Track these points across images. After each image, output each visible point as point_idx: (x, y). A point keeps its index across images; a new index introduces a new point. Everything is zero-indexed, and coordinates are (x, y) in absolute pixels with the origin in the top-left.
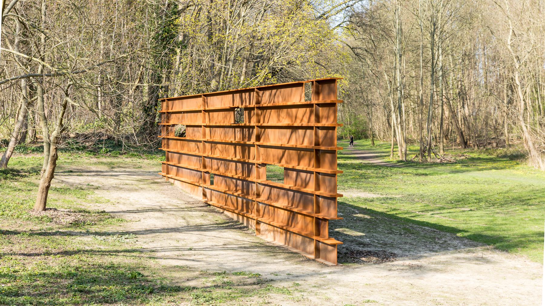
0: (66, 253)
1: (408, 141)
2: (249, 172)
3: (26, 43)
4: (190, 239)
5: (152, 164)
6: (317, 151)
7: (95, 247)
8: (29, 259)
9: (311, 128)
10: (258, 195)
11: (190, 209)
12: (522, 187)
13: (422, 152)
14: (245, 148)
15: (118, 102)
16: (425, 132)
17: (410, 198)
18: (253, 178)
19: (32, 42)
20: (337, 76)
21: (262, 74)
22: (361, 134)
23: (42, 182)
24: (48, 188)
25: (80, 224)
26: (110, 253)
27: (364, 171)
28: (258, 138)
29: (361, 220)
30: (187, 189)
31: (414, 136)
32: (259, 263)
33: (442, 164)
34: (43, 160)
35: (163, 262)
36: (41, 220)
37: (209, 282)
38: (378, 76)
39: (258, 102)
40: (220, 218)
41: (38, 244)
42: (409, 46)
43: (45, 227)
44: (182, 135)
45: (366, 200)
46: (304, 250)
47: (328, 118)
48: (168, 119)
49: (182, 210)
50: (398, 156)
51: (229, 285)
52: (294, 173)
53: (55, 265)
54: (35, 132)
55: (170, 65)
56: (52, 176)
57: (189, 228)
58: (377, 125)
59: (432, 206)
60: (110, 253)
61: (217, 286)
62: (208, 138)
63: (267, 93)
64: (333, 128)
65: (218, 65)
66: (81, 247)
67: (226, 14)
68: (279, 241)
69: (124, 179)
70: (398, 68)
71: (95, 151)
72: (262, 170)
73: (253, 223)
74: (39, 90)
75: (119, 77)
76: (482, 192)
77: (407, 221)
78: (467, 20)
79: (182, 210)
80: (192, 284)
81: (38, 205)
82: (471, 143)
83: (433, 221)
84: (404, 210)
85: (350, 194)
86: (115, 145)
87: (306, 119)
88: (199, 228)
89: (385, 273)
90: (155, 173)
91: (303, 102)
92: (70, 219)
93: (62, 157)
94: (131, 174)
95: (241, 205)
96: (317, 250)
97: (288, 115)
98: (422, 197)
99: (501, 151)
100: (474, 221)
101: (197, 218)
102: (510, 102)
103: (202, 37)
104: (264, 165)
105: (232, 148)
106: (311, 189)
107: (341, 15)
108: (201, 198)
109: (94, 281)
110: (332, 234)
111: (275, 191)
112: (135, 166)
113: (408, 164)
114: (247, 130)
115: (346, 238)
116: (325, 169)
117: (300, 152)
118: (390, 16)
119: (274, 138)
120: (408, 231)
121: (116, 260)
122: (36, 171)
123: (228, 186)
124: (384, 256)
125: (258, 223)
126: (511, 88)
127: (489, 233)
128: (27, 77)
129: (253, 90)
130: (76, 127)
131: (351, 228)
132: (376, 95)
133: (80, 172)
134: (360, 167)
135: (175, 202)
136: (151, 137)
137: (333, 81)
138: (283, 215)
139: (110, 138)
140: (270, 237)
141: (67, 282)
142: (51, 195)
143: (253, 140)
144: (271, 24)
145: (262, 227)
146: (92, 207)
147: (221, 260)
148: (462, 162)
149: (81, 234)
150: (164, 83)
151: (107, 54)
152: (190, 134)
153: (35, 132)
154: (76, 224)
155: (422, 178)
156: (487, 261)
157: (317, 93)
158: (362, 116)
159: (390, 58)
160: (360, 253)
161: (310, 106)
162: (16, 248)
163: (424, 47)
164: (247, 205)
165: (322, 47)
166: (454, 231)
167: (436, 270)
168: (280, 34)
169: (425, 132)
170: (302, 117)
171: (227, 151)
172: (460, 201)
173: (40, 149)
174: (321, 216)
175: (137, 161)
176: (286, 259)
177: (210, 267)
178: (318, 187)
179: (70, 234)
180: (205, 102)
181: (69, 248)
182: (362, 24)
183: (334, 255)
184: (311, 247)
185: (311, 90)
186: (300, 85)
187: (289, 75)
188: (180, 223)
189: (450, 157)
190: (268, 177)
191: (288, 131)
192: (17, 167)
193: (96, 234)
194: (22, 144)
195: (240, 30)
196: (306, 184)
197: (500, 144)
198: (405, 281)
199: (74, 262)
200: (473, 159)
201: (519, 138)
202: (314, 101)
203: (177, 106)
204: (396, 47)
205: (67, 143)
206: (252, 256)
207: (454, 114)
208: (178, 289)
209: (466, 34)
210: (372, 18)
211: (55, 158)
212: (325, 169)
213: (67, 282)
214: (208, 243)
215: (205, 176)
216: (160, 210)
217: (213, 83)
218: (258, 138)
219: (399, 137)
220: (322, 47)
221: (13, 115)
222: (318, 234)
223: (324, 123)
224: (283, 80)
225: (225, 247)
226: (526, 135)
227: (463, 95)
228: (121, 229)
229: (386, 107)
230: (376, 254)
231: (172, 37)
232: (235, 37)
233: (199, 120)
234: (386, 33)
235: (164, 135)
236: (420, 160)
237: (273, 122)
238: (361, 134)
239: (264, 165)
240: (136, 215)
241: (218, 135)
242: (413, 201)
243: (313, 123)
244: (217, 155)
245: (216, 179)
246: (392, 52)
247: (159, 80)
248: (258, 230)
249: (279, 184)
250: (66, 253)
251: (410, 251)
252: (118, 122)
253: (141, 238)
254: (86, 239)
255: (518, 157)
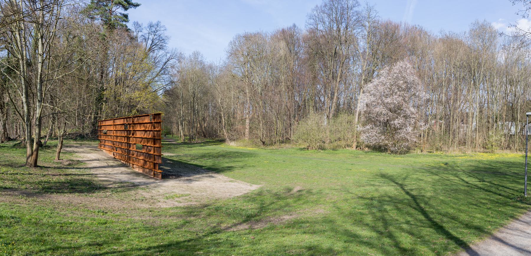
0: (66, 175)
1: (185, 135)
2: (130, 147)
3: (52, 102)
4: (109, 170)
5: (95, 144)
6: (154, 139)
7: (76, 173)
8: (54, 177)
9: (152, 131)
10: (133, 155)
11: (109, 160)
12: (223, 151)
13: (190, 139)
14: (128, 138)
15: (83, 122)
16: (191, 132)
17: (186, 156)
18: (131, 149)
19: (54, 101)
20: (160, 112)
21: (134, 111)
22: (169, 133)
23: (58, 150)
24: (60, 152)
25: (72, 164)
26: (81, 175)
27: (170, 147)
28: (133, 135)
29: (169, 163)
30: (108, 153)
31: (187, 134)
32: (133, 179)
33: (197, 143)
34: (58, 142)
35: (100, 179)
36: (58, 163)
37: (116, 185)
38: (175, 112)
39: (133, 122)
40: (119, 163)
41: (57, 171)
42: (185, 102)
43: (59, 165)
44: (105, 133)
45: (171, 156)
46: (150, 174)
47: (158, 127)
48: (101, 128)
49: (106, 160)
50: (182, 141)
51: (122, 187)
52: (146, 147)
53: (63, 179)
54: (55, 133)
55: (101, 109)
56: (61, 148)
57: (108, 167)
58: (174, 130)
59: (194, 158)
60: (81, 175)
61: (119, 187)
62: (115, 134)
63: (136, 119)
64: (160, 131)
65: (118, 108)
66: (71, 173)
67: (121, 90)
68: (141, 171)
69: (86, 149)
70: (182, 110)
71: (75, 140)
72: (134, 146)
73: (131, 165)
74: (56, 118)
75: (84, 113)
76: (210, 153)
77: (185, 163)
78: (205, 93)
79: (106, 160)
80: (110, 186)
81: (56, 158)
82: (207, 136)
83: (194, 163)
84: (184, 159)
85: (166, 154)
86: (81, 137)
87: (150, 128)
88: (112, 166)
89: (178, 182)
90: (96, 147)
91: (149, 121)
92: (67, 163)
93: (64, 142)
94: (88, 147)
95: (126, 158)
96: (154, 174)
97: (144, 126)
98: (190, 155)
99: (217, 139)
100: (209, 163)
101: (111, 163)
102: (220, 122)
103: (112, 98)
104: (135, 144)
105: (123, 138)
106: (152, 152)
107: (161, 91)
108: (112, 156)
109: (76, 185)
110: (160, 169)
111: (139, 153)
112: (89, 144)
113: (185, 143)
114: (129, 132)
115: (164, 170)
116: (157, 145)
117: (148, 140)
118: (179, 91)
119: (138, 134)
120: (186, 167)
121: (84, 177)
122: (56, 146)
123: (122, 152)
124: (177, 176)
125: (133, 165)
126: (221, 117)
127: (213, 167)
128: (53, 114)
129: (130, 118)
130: (69, 131)
131: (166, 166)
132: (174, 119)
133: (70, 147)
134: (168, 144)
135: (103, 157)
136: (94, 135)
137: (160, 114)
138: (142, 161)
139: (80, 135)
140: (137, 170)
141: (67, 185)
142: (61, 155)
143: (131, 135)
144: (137, 93)
145: (135, 166)
146: (75, 159)
147: (120, 178)
148: (203, 143)
149: (71, 168)
150: (99, 115)
151: (79, 105)
152: (108, 133)
153: (55, 133)
154: (69, 165)
155: (190, 149)
156: (213, 177)
157: (154, 119)
158: (169, 127)
159: (178, 106)
160: (170, 175)
161: (152, 123)
162: (50, 173)
163: (191, 102)
164: (129, 158)
165: (155, 102)
166: (201, 167)
167: (196, 181)
168: (140, 97)
169: (191, 132)
170: (149, 127)
171: (122, 139)
172: (203, 156)
173: (57, 139)
174: (155, 162)
175: (90, 142)
176: (143, 177)
177: (117, 180)
178: (154, 152)
179: (68, 168)
180: (114, 122)
181: (67, 173)
182: (169, 94)
183: (160, 176)
184: (152, 173)
185: (152, 117)
186: (148, 115)
187: (143, 112)
188: (105, 164)
189: (199, 141)
190: (137, 148)
191: (144, 132)
192: (49, 145)
193: (76, 168)
194: (51, 138)
195: (126, 96)
196: (150, 151)
197: (217, 136)
198: (185, 185)
199: (69, 178)
200: (207, 142)
201: (223, 134)
202: (153, 121)
203: (104, 124)
204: (181, 102)
205: (66, 137)
206: (131, 176)
207: (201, 126)
208: (106, 188)
209: (205, 98)
210: (173, 92)
211: (62, 142)
212: (157, 145)
213: (67, 185)
214: (115, 172)
215: (113, 148)
216: (98, 160)
217: (116, 115)
218: (133, 135)
219: (182, 134)
220: (155, 102)
221: (47, 127)
222: (155, 168)
223: (157, 129)
224: (142, 114)
225: (122, 173)
226: (225, 134)
227: (204, 119)
228: (85, 167)
229: (177, 123)
230: (175, 175)
231: (102, 99)
232: (124, 98)
233: (112, 128)
234: (178, 97)
235: (99, 133)
236: (189, 142)
237: (138, 129)
238: (169, 133)
239: (135, 144)
240: (90, 162)
241: (119, 134)
242: (187, 157)
243: (153, 129)
244: (118, 140)
245: (118, 149)
246: (179, 104)
247: (97, 114)
248: (133, 167)
249: (140, 151)
250: (66, 175)
251: (187, 174)
252: (83, 129)
253: (92, 170)
254: (73, 170)
255: (223, 141)
